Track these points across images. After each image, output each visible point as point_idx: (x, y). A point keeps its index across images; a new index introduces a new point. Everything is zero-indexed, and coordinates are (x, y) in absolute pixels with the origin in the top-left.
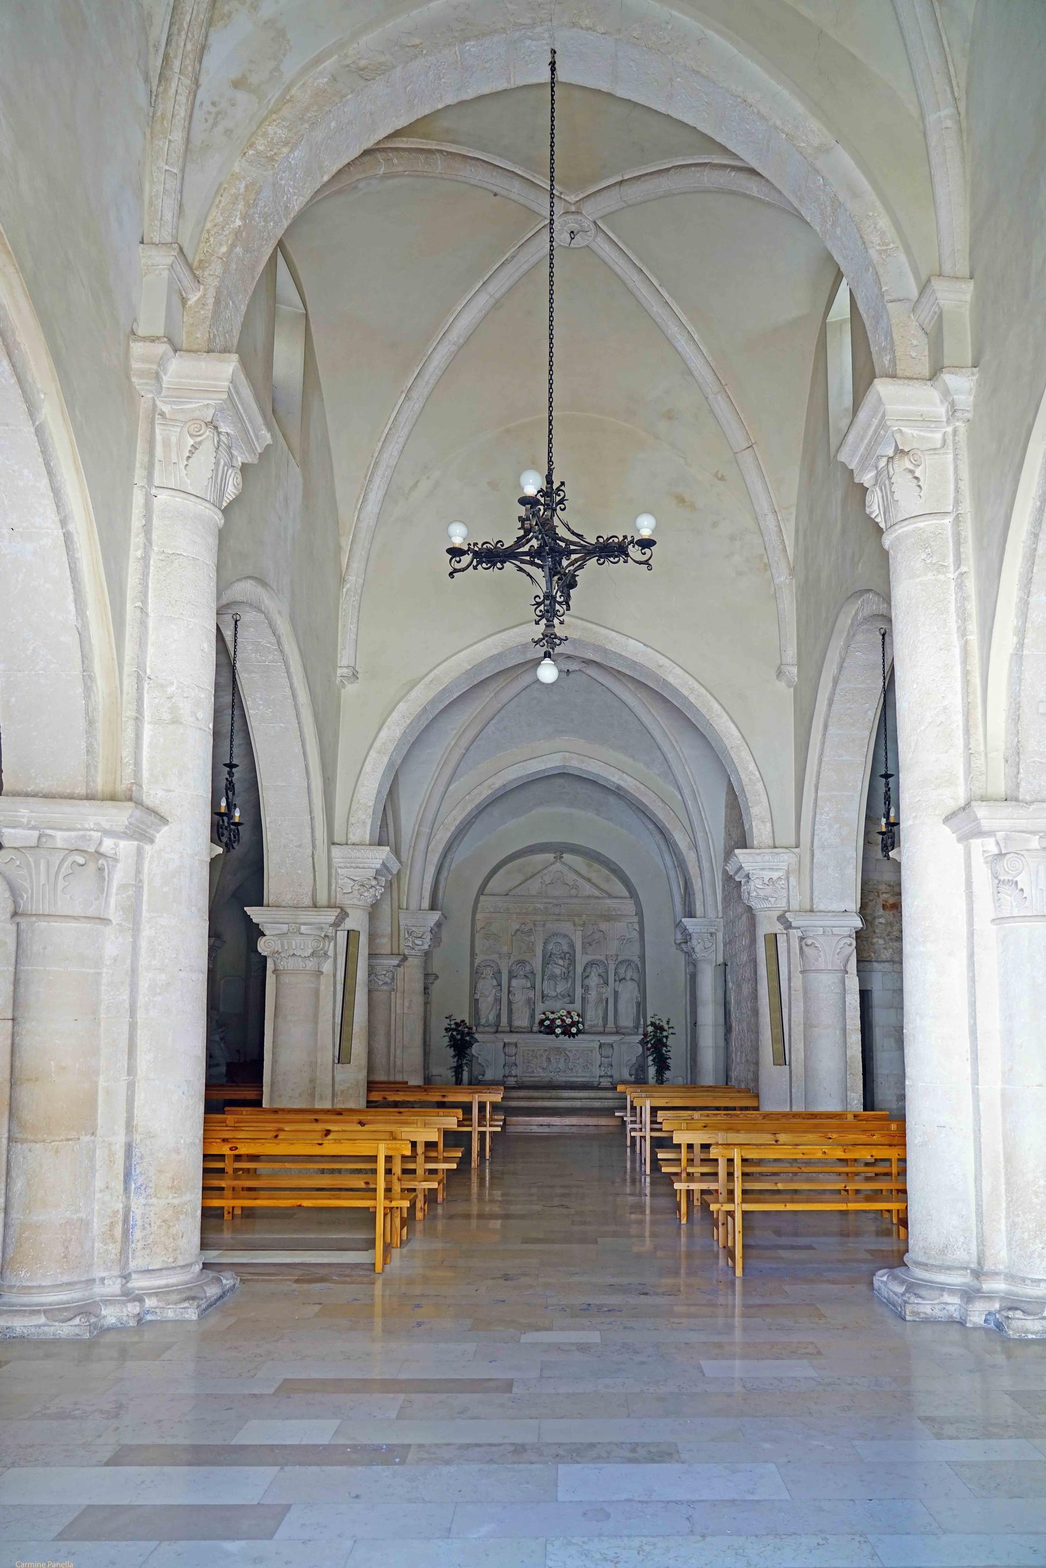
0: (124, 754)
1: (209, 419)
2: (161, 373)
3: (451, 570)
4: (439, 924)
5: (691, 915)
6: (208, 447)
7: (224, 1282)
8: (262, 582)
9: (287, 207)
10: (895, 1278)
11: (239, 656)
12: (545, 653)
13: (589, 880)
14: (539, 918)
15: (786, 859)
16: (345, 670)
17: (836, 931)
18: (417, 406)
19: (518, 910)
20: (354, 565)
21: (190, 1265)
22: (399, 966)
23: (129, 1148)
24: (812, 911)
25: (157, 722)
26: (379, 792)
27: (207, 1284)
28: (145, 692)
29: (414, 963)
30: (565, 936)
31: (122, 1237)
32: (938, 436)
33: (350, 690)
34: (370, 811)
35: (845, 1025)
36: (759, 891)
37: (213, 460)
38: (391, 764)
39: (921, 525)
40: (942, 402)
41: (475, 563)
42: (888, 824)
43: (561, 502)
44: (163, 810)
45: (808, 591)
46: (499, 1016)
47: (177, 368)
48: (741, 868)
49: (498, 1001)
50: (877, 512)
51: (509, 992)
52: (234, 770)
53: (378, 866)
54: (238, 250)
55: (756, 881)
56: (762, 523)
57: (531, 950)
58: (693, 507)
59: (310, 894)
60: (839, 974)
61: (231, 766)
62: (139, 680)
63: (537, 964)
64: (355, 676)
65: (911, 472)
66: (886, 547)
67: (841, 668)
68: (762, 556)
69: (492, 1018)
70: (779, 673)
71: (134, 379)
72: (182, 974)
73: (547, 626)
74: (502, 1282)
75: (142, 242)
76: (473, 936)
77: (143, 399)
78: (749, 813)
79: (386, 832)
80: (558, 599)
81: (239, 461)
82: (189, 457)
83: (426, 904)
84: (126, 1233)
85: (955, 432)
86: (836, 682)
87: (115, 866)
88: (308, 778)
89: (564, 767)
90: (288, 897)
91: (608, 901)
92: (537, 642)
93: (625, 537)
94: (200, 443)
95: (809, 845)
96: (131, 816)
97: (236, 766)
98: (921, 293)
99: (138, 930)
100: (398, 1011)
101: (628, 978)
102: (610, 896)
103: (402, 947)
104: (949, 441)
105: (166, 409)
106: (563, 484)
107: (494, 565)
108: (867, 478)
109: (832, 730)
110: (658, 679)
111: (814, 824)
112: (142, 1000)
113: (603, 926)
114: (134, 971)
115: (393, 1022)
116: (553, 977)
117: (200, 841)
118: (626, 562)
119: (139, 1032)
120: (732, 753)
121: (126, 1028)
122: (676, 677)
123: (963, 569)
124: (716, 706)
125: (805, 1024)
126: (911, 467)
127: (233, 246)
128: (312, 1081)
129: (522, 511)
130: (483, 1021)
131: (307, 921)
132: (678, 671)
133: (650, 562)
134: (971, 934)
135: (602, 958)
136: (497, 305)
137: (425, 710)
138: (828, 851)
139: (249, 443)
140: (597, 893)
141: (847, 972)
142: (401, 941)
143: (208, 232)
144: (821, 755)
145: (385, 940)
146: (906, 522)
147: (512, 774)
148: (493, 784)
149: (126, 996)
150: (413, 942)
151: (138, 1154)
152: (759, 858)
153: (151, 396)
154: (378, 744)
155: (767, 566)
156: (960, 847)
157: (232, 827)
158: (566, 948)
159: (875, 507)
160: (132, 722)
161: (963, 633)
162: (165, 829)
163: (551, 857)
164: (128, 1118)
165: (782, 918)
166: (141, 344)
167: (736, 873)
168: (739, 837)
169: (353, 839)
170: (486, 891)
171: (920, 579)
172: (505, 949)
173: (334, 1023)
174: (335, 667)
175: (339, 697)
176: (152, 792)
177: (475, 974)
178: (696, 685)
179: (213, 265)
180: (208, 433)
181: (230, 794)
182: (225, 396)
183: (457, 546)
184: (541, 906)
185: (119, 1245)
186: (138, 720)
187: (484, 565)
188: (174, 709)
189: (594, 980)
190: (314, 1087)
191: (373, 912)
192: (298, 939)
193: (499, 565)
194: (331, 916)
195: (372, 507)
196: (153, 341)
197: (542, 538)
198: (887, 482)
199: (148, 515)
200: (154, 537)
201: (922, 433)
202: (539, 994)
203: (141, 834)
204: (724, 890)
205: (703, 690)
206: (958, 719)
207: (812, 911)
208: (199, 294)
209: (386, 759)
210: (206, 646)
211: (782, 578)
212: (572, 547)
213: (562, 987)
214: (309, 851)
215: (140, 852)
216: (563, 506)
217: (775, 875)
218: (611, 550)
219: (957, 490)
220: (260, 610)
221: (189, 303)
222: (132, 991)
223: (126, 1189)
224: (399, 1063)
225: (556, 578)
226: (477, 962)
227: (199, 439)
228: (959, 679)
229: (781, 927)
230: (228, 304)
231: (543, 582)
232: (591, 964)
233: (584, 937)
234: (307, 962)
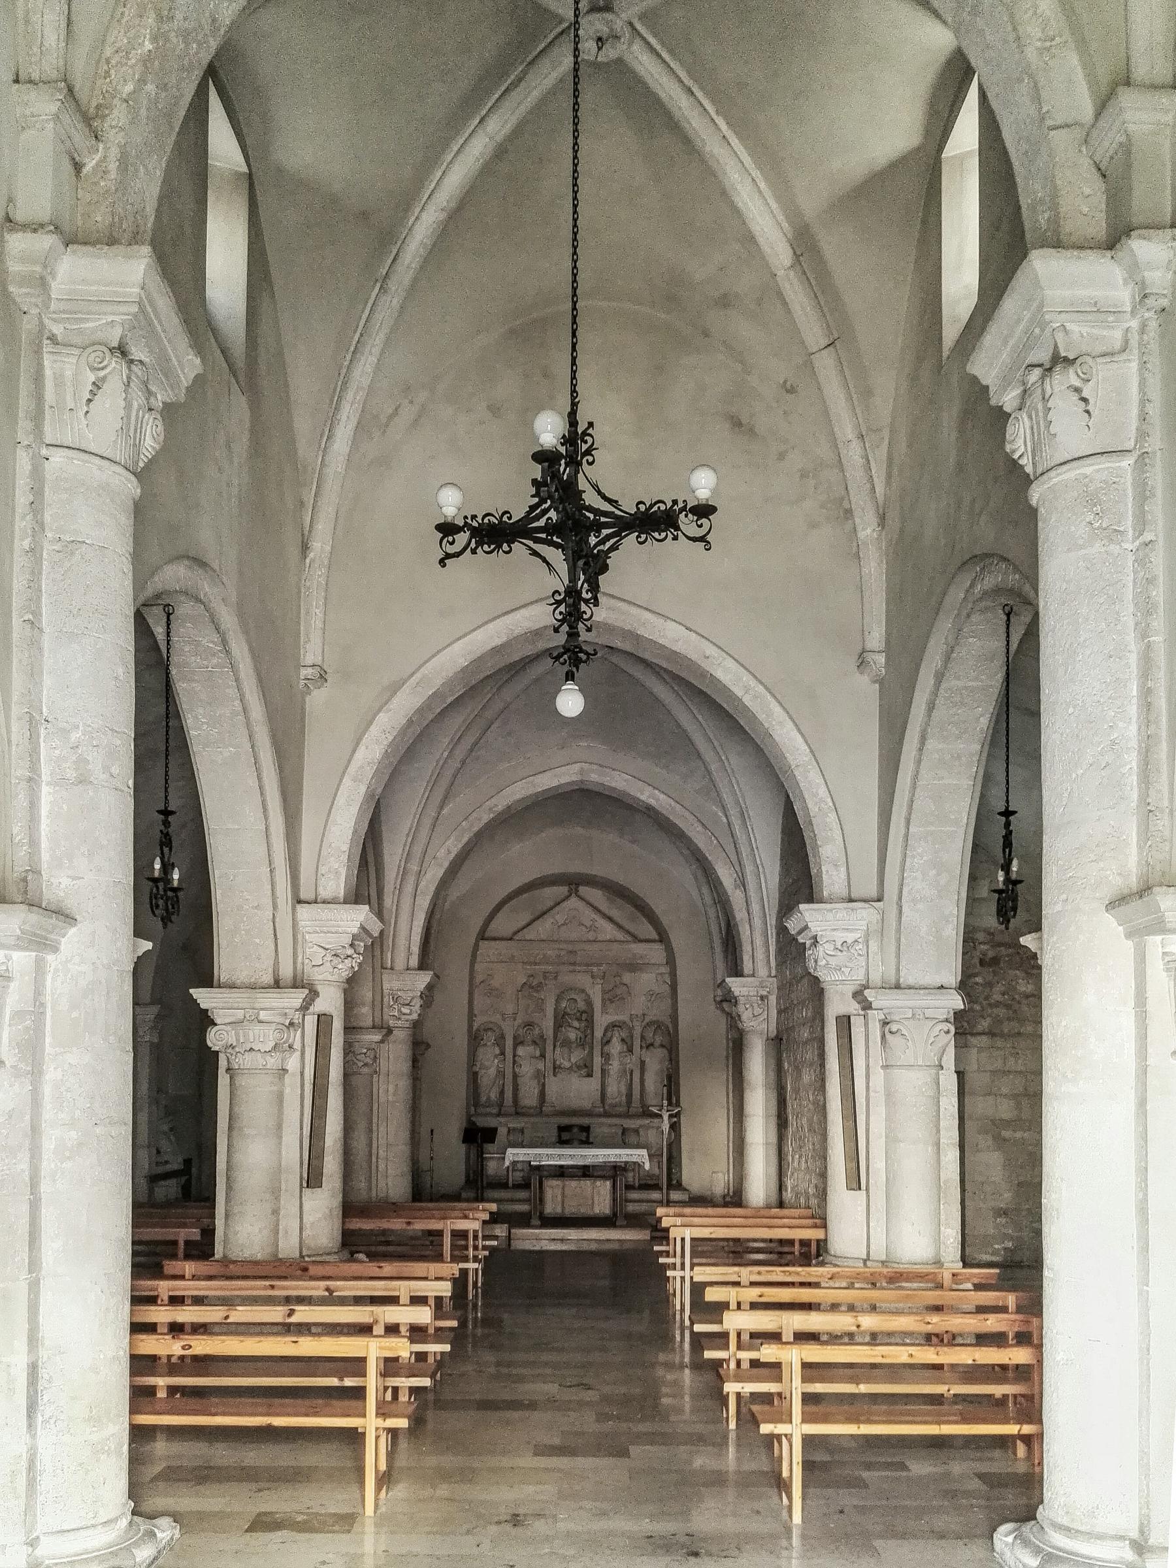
0: (15, 830)
1: (115, 344)
2: (49, 278)
3: (441, 555)
4: (430, 987)
5: (737, 972)
6: (114, 385)
7: (159, 1535)
8: (200, 563)
9: (214, 20)
10: (1026, 1543)
11: (174, 659)
12: (567, 673)
13: (610, 919)
15: (865, 915)
16: (310, 670)
17: (929, 1013)
18: (395, 301)
20: (319, 527)
21: (115, 1520)
22: (382, 1041)
23: (33, 1370)
24: (898, 987)
25: (60, 782)
26: (355, 832)
27: (136, 1544)
28: (41, 740)
29: (401, 1035)
31: (27, 1490)
32: (1118, 335)
33: (317, 699)
34: (345, 858)
36: (829, 958)
37: (123, 404)
38: (370, 795)
39: (1088, 470)
40: (1126, 283)
41: (473, 545)
42: (1008, 880)
43: (588, 452)
44: (71, 904)
45: (903, 550)
46: (502, 1093)
47: (75, 271)
48: (806, 927)
49: (501, 1074)
50: (1022, 449)
51: (514, 1062)
52: (170, 818)
53: (355, 931)
54: (150, 87)
55: (826, 946)
56: (843, 452)
57: (541, 1009)
58: (752, 432)
59: (271, 970)
60: (934, 1071)
61: (166, 813)
62: (32, 725)
63: (548, 1025)
64: (323, 677)
65: (1077, 390)
66: (1034, 502)
67: (947, 658)
68: (843, 499)
69: (494, 1096)
70: (862, 664)
71: (11, 289)
72: (98, 1130)
73: (570, 635)
74: (508, 1527)
75: (17, 81)
76: (471, 994)
77: (25, 317)
78: (817, 855)
79: (367, 883)
80: (584, 595)
81: (158, 401)
82: (89, 401)
83: (414, 961)
84: (32, 1483)
85: (1143, 329)
86: (939, 677)
87: (8, 987)
88: (266, 818)
89: (582, 782)
90: (245, 973)
91: (633, 946)
93: (675, 502)
94: (104, 379)
95: (895, 898)
96: (24, 923)
97: (172, 813)
98: (1098, 115)
99: (41, 1073)
100: (381, 1100)
101: (657, 1043)
102: (636, 939)
103: (385, 1017)
104: (1134, 339)
105: (57, 329)
106: (591, 425)
107: (499, 546)
108: (1008, 399)
109: (931, 744)
110: (704, 674)
111: (903, 870)
112: (48, 1164)
113: (627, 977)
114: (35, 1130)
116: (566, 1043)
117: (119, 944)
118: (675, 538)
119: (43, 1211)
120: (796, 773)
121: (25, 1208)
122: (727, 673)
123: (1148, 536)
124: (777, 709)
126: (1077, 383)
127: (142, 81)
129: (537, 471)
130: (483, 1099)
132: (730, 663)
133: (709, 538)
134: (1143, 1071)
136: (500, 152)
137: (410, 722)
138: (920, 906)
139: (168, 372)
140: (620, 936)
142: (385, 1010)
143: (108, 61)
144: (916, 777)
145: (365, 1010)
146: (1065, 468)
147: (518, 792)
149: (24, 1166)
150: (399, 1011)
151: (46, 1376)
152: (830, 916)
153: (35, 311)
154: (352, 769)
155: (849, 513)
156: (1130, 944)
157: (170, 894)
158: (582, 1005)
159: (1019, 440)
160: (24, 784)
161: (1144, 633)
162: (73, 931)
163: (563, 890)
164: (30, 1330)
165: (858, 995)
166: (20, 235)
167: (800, 933)
168: (800, 883)
169: (324, 893)
170: (487, 935)
171: (1083, 552)
172: (510, 1008)
173: (301, 1134)
174: (299, 666)
175: (303, 709)
176: (54, 881)
177: (475, 1039)
178: (753, 683)
179: (115, 112)
180: (114, 364)
181: (166, 850)
182: (135, 309)
183: (449, 520)
185: (22, 1501)
186: (33, 781)
187: (486, 547)
188: (81, 761)
189: (616, 1047)
190: (278, 1220)
191: (351, 984)
192: (257, 1029)
193: (505, 547)
194: (296, 998)
195: (341, 443)
196: (35, 231)
197: (564, 509)
198: (1040, 406)
199: (37, 491)
200: (47, 518)
201: (1095, 331)
202: (550, 1065)
203: (42, 943)
204: (778, 941)
206: (1132, 761)
208: (97, 157)
209: (363, 789)
210: (120, 671)
211: (867, 530)
212: (603, 519)
213: (577, 1056)
215: (40, 969)
216: (590, 459)
217: (850, 937)
218: (655, 521)
219: (1143, 417)
220: (198, 600)
221: (85, 171)
222: (32, 1157)
223: (31, 1426)
224: (382, 1167)
225: (581, 563)
227: (102, 374)
228: (1135, 701)
229: (857, 1006)
230: (137, 170)
231: (562, 568)
232: (613, 1026)
233: (604, 992)
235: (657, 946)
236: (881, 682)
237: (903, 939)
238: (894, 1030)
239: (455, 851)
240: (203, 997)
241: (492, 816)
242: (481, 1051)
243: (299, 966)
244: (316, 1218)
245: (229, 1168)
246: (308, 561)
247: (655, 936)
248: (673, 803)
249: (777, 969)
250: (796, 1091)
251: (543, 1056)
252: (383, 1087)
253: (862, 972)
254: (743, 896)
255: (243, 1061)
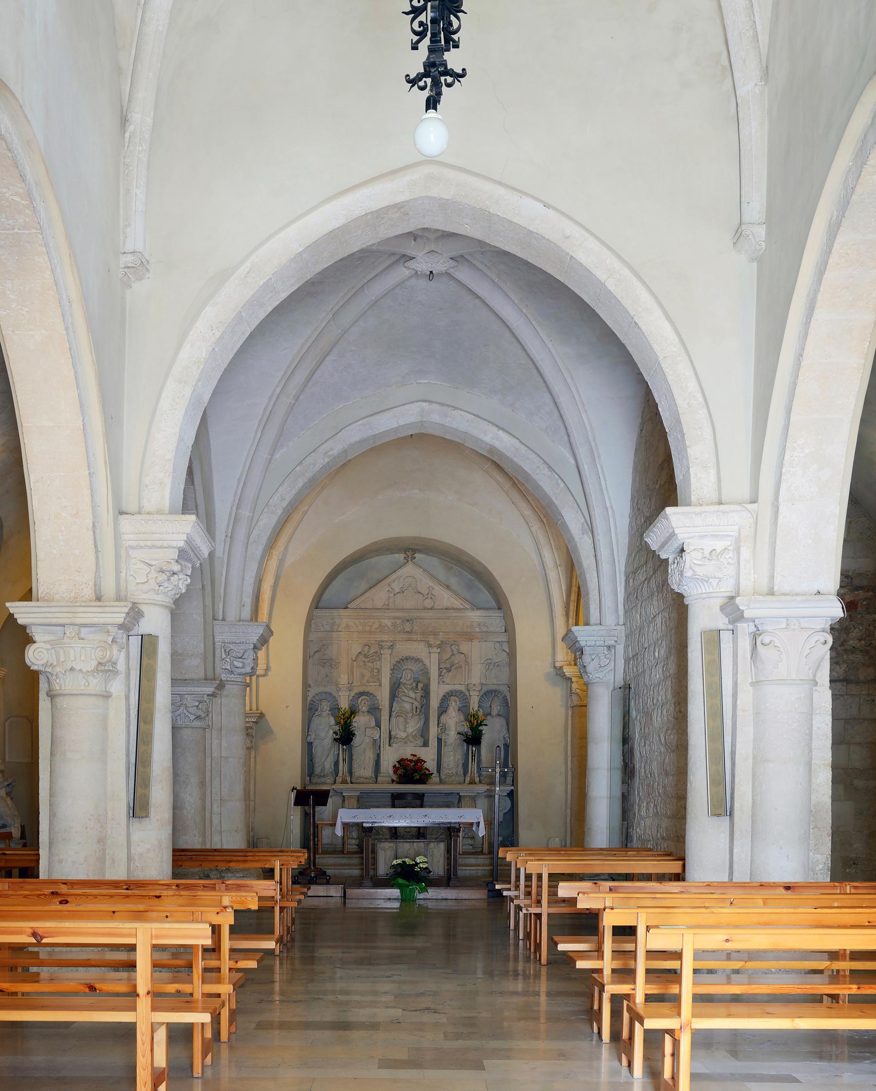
13: (448, 587)
14: (385, 637)
15: (737, 520)
19: (360, 628)
22: (213, 695)
24: (771, 593)
26: (181, 440)
30: (418, 660)
35: (811, 758)
48: (673, 535)
53: (181, 544)
59: (91, 583)
63: (383, 696)
70: (738, 234)
79: (196, 490)
83: (247, 613)
92: (413, 82)
100: (215, 755)
103: (218, 670)
109: (820, 314)
115: (208, 768)
125: (755, 758)
128: (101, 840)
130: (318, 770)
131: (88, 621)
132: (592, 244)
135: (462, 688)
141: (816, 684)
144: (800, 356)
148: (331, 449)
163: (401, 557)
167: (662, 546)
170: (320, 605)
184: (388, 622)
190: (104, 850)
202: (385, 736)
205: (626, 272)
207: (771, 593)
209: (188, 391)
211: (749, 83)
214: (89, 522)
217: (719, 545)
224: (216, 821)
226: (311, 695)
234: (90, 678)
235: (497, 614)
236: (760, 260)
237: (778, 543)
238: (767, 641)
239: (288, 498)
240: (22, 612)
241: (327, 460)
242: (316, 720)
243: (123, 584)
244: (147, 851)
245: (52, 794)
246: (127, 135)
247: (493, 604)
248: (518, 445)
249: (625, 617)
250: (645, 737)
251: (378, 725)
252: (215, 742)
253: (732, 582)
254: (590, 541)
255: (65, 683)
